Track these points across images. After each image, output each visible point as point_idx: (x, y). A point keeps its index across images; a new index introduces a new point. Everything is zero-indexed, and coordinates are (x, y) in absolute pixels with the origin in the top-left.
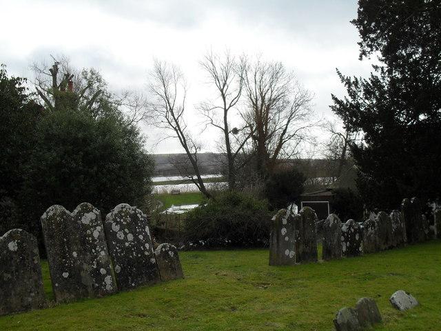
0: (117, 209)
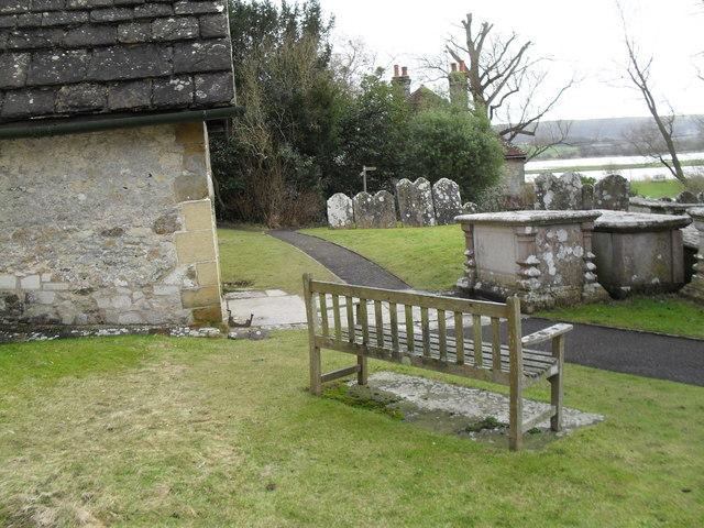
0: (439, 182)
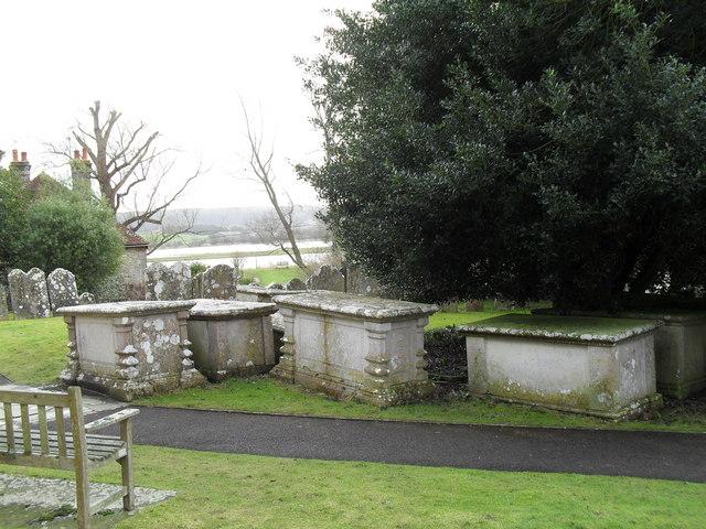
0: (54, 272)
